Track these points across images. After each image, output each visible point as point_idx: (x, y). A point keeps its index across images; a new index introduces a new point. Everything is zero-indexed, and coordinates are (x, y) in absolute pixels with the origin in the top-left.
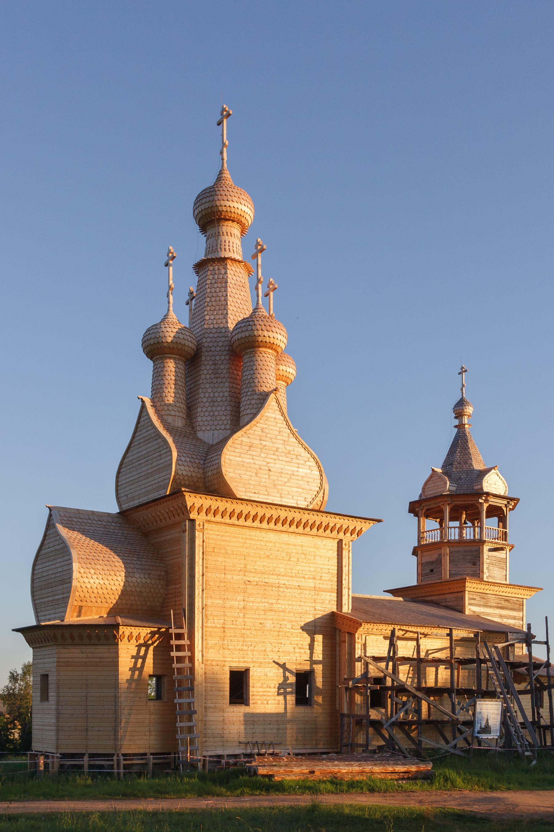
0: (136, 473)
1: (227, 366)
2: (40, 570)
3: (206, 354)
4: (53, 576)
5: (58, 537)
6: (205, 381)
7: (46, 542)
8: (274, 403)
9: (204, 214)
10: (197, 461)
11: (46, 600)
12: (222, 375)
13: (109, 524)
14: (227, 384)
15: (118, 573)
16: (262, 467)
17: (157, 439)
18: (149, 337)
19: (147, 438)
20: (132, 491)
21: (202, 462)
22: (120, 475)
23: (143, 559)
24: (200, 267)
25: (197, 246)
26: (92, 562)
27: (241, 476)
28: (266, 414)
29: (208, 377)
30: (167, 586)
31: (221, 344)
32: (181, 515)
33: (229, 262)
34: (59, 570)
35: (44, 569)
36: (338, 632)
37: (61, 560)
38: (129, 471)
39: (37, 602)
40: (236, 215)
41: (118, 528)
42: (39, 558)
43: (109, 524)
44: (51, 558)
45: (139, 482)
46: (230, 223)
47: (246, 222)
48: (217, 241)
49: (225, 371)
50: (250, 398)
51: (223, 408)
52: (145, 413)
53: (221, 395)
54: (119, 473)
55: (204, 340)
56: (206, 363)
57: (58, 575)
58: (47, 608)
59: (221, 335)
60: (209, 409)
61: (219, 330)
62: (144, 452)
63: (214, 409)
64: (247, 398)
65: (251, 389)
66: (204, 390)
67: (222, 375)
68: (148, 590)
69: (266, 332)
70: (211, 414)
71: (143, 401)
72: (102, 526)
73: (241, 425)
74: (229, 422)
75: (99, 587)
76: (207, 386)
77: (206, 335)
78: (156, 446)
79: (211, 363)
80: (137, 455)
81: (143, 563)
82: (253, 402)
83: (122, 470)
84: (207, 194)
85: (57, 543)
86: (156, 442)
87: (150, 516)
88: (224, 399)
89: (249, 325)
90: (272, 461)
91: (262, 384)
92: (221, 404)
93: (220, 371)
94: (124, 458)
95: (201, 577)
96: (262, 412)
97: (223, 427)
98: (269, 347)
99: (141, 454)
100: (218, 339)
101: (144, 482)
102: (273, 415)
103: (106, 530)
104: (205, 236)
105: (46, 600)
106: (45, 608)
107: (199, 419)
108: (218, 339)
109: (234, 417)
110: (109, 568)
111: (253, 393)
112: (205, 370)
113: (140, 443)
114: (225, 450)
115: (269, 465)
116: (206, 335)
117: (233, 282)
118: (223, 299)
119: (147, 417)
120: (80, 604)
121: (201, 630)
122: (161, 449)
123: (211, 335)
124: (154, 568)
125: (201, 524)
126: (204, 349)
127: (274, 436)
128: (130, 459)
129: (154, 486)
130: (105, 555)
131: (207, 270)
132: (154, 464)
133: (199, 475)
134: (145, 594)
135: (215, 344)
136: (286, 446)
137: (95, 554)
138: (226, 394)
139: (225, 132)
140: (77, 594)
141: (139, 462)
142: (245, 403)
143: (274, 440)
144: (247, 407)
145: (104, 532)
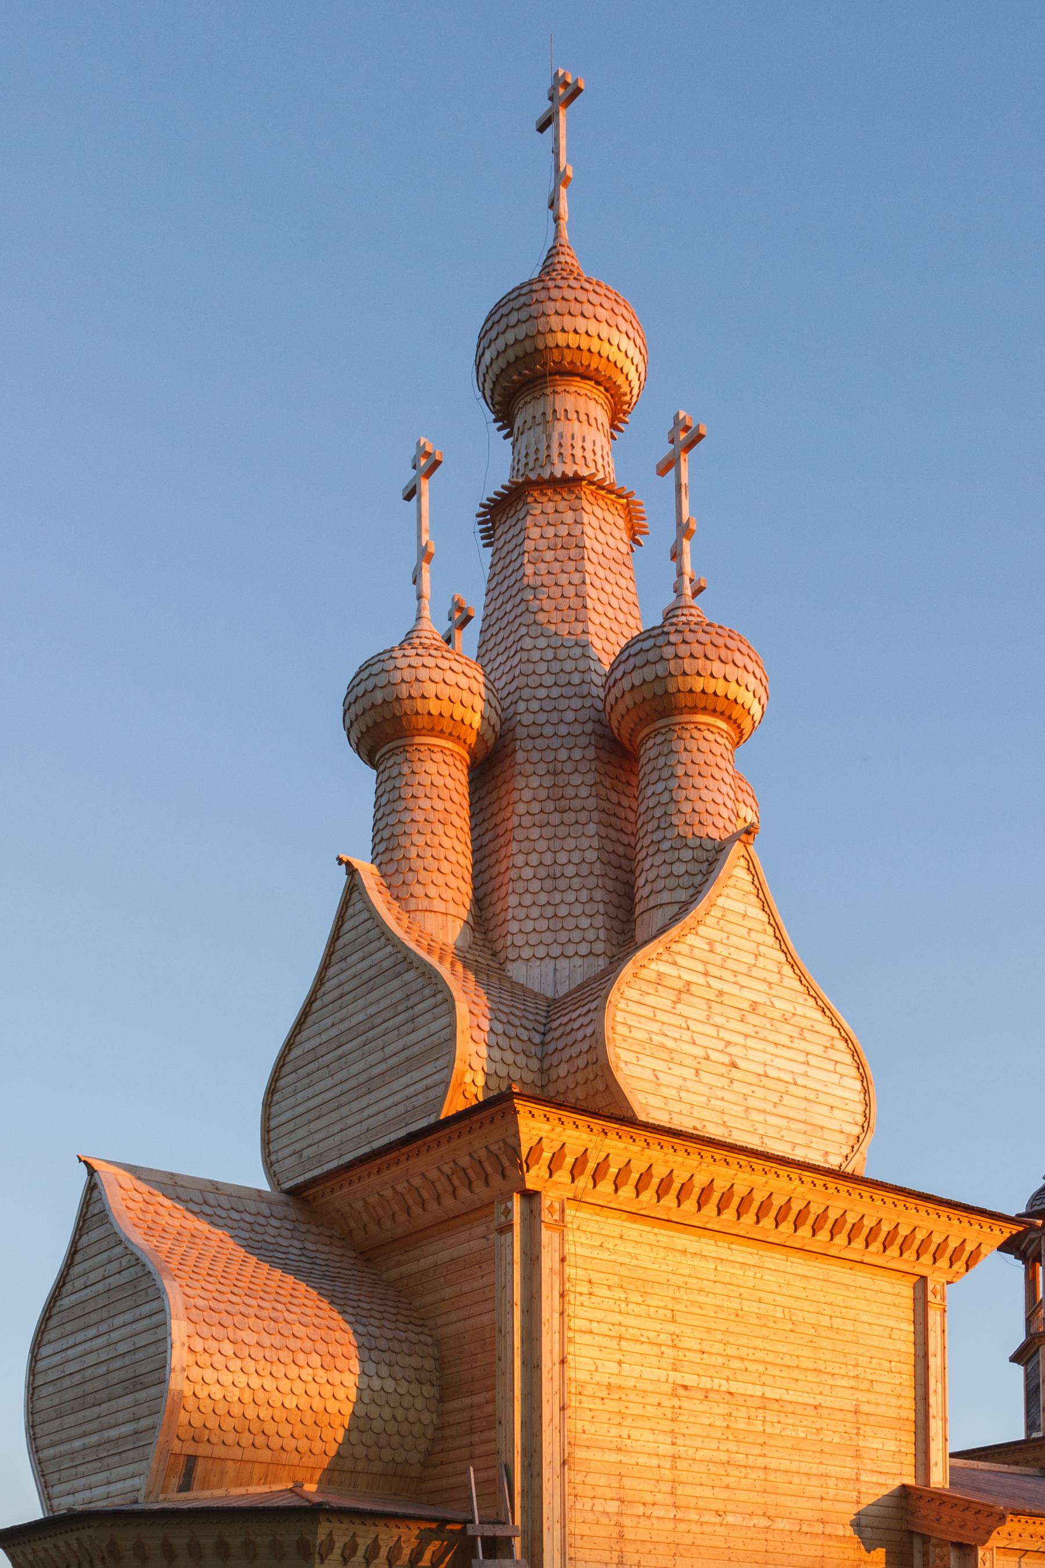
0: (329, 1082)
1: (590, 778)
2: (56, 1359)
3: (529, 744)
4: (103, 1369)
5: (118, 1250)
6: (527, 821)
7: (76, 1270)
8: (741, 873)
9: (512, 359)
10: (524, 1035)
11: (77, 1444)
12: (577, 804)
13: (262, 1221)
14: (591, 829)
15: (301, 1358)
16: (711, 1053)
17: (400, 974)
18: (369, 685)
19: (365, 977)
20: (317, 1137)
21: (537, 1038)
22: (277, 1097)
23: (372, 1320)
24: (501, 511)
25: (487, 458)
26: (227, 1320)
27: (659, 1074)
28: (720, 901)
29: (536, 807)
30: (441, 1401)
31: (569, 716)
32: (496, 1180)
33: (587, 489)
34: (122, 1348)
35: (70, 1352)
36: (917, 1544)
37: (128, 1316)
38: (306, 1081)
39: (45, 1454)
40: (604, 360)
41: (288, 1234)
42: (52, 1323)
43: (262, 1221)
44: (95, 1317)
45: (342, 1106)
46: (586, 387)
47: (625, 388)
48: (549, 437)
49: (584, 792)
50: (668, 857)
51: (584, 895)
52: (360, 905)
53: (576, 857)
54: (272, 1090)
55: (521, 707)
56: (528, 768)
57: (118, 1363)
58: (81, 1469)
59: (569, 691)
60: (543, 898)
61: (563, 679)
62: (355, 1020)
63: (557, 897)
64: (658, 860)
65: (669, 833)
66: (526, 846)
67: (577, 804)
68: (387, 1413)
69: (717, 664)
70: (549, 911)
71: (351, 871)
72: (242, 1224)
73: (639, 937)
74: (602, 934)
75: (247, 1398)
76: (535, 833)
77: (526, 693)
78: (399, 995)
79: (542, 769)
80: (334, 1032)
81: (371, 1329)
82: (679, 869)
83: (282, 1083)
84: (522, 300)
85: (113, 1267)
86: (396, 983)
87: (388, 1193)
88: (585, 869)
89: (669, 643)
90: (740, 1039)
91: (705, 817)
92: (576, 882)
93: (570, 792)
94: (289, 1045)
95: (557, 1366)
96: (712, 892)
97: (584, 949)
98: (722, 713)
99: (343, 1027)
100: (563, 704)
101: (355, 1106)
102: (740, 908)
103: (254, 1236)
104: (506, 437)
105: (77, 1444)
106: (73, 1471)
107: (514, 927)
108: (563, 704)
109: (614, 922)
110: (277, 1340)
111: (678, 843)
112: (526, 794)
113: (342, 996)
114: (614, 996)
115: (731, 1049)
116: (526, 693)
117: (599, 548)
118: (570, 591)
119: (365, 915)
120: (190, 1449)
121: (558, 1526)
122: (413, 1000)
123: (542, 693)
124: (405, 1346)
125: (557, 1206)
126: (521, 732)
127: (743, 969)
128: (309, 1045)
129: (392, 1113)
130: (262, 1303)
131: (522, 515)
132: (389, 1051)
133: (529, 1077)
134: (378, 1426)
135: (554, 717)
136: (774, 1000)
137: (234, 1299)
138: (591, 856)
139: (563, 143)
140: (183, 1417)
141: (340, 1051)
142: (652, 876)
143: (743, 980)
144: (660, 884)
145: (250, 1243)
